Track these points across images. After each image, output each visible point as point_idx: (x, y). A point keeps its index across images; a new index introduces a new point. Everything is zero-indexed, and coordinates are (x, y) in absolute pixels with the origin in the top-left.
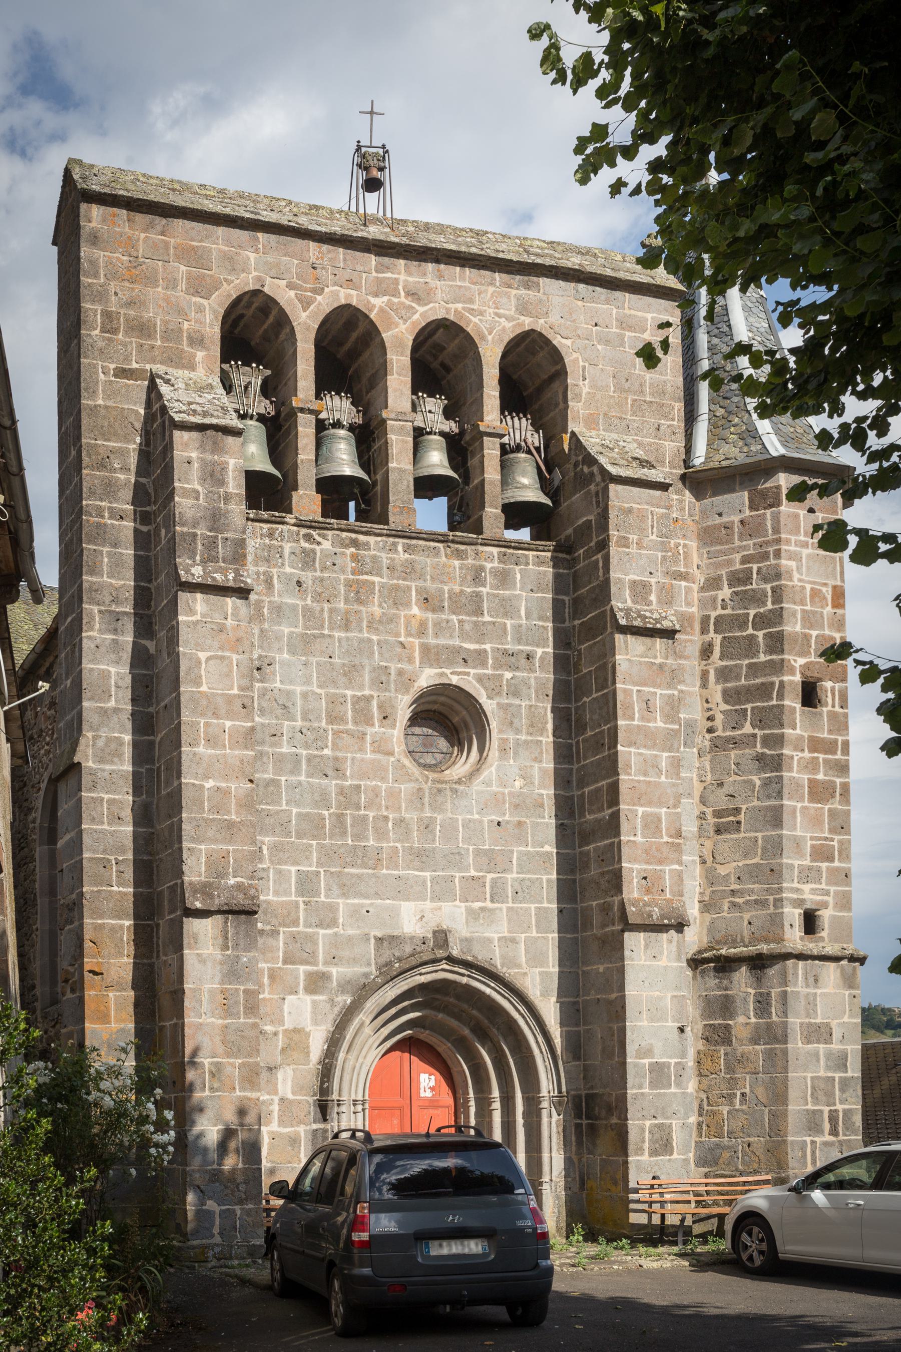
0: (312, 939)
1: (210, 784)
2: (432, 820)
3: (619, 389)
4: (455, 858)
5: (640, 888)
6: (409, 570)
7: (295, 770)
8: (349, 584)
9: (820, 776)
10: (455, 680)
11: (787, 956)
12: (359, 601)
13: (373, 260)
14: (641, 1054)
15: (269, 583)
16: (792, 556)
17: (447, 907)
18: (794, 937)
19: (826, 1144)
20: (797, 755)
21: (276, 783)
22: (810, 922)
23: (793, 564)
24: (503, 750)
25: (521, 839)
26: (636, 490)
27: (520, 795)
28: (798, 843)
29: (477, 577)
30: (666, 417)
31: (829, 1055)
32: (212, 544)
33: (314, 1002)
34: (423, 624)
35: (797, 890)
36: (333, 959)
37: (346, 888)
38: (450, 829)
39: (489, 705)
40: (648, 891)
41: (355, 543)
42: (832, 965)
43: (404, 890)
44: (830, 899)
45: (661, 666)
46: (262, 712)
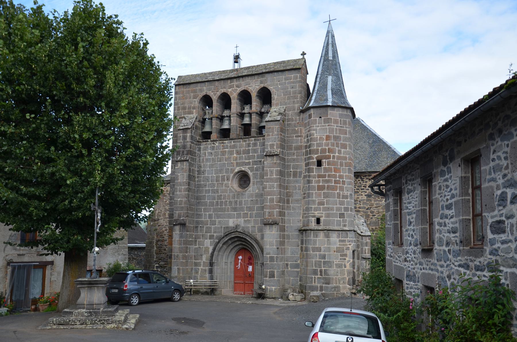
0: (211, 228)
1: (179, 200)
2: (237, 201)
3: (284, 95)
4: (242, 209)
5: (268, 215)
6: (234, 147)
7: (209, 193)
8: (221, 152)
9: (321, 184)
10: (243, 169)
11: (311, 230)
12: (223, 155)
13: (229, 81)
14: (267, 254)
15: (205, 154)
16: (316, 130)
17: (239, 220)
18: (313, 225)
19: (318, 278)
20: (314, 180)
21: (205, 196)
22: (318, 221)
23: (315, 132)
24: (253, 184)
25: (257, 203)
26: (272, 123)
27: (257, 193)
28: (314, 201)
29: (249, 145)
30: (296, 99)
31: (320, 255)
32: (183, 152)
33: (211, 242)
34: (237, 158)
35: (313, 213)
36: (215, 232)
37: (218, 217)
38: (241, 203)
39: (250, 174)
40: (270, 216)
41: (223, 143)
42: (322, 232)
43: (230, 217)
44: (323, 215)
45: (275, 163)
46: (203, 181)
